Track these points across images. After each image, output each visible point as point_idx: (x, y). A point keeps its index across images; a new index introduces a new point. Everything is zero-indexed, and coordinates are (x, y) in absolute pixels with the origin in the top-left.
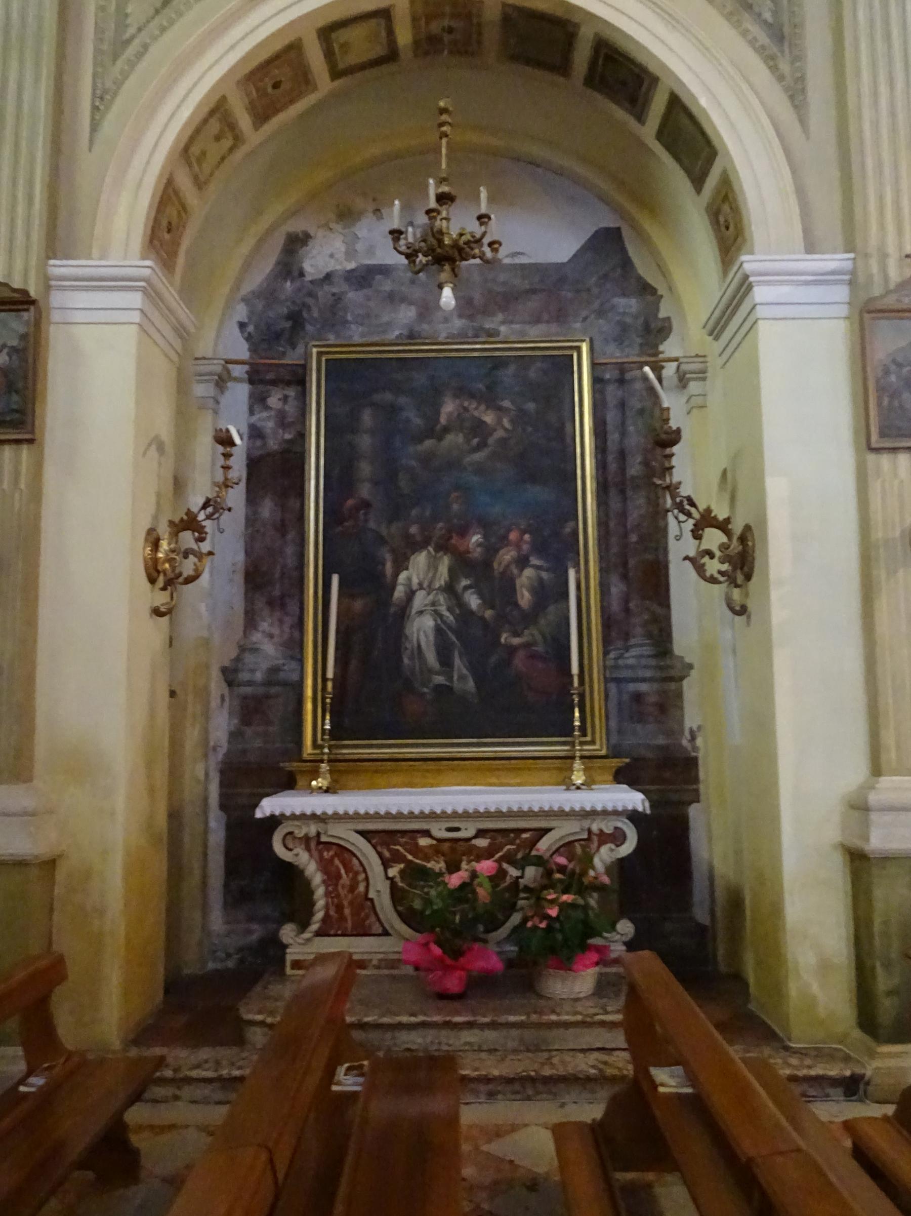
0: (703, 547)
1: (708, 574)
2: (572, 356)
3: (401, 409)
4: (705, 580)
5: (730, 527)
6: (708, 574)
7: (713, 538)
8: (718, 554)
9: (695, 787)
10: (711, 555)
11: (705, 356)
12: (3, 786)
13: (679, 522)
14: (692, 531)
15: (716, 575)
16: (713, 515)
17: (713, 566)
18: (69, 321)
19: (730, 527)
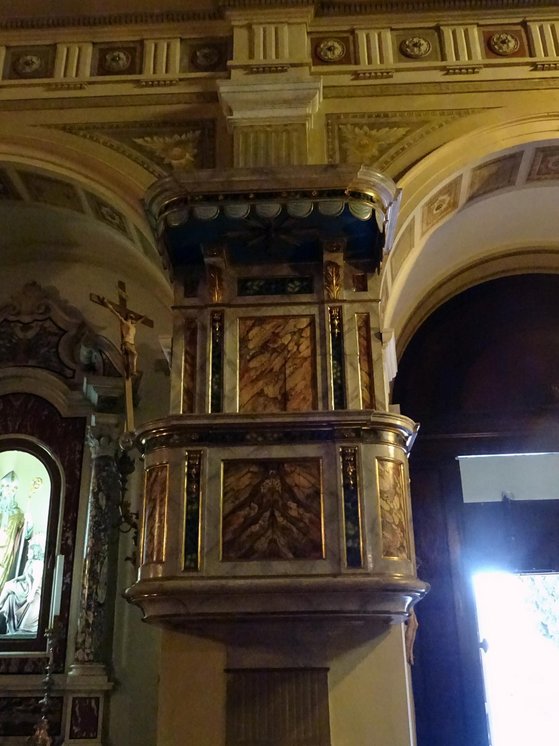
11: (26, 601)
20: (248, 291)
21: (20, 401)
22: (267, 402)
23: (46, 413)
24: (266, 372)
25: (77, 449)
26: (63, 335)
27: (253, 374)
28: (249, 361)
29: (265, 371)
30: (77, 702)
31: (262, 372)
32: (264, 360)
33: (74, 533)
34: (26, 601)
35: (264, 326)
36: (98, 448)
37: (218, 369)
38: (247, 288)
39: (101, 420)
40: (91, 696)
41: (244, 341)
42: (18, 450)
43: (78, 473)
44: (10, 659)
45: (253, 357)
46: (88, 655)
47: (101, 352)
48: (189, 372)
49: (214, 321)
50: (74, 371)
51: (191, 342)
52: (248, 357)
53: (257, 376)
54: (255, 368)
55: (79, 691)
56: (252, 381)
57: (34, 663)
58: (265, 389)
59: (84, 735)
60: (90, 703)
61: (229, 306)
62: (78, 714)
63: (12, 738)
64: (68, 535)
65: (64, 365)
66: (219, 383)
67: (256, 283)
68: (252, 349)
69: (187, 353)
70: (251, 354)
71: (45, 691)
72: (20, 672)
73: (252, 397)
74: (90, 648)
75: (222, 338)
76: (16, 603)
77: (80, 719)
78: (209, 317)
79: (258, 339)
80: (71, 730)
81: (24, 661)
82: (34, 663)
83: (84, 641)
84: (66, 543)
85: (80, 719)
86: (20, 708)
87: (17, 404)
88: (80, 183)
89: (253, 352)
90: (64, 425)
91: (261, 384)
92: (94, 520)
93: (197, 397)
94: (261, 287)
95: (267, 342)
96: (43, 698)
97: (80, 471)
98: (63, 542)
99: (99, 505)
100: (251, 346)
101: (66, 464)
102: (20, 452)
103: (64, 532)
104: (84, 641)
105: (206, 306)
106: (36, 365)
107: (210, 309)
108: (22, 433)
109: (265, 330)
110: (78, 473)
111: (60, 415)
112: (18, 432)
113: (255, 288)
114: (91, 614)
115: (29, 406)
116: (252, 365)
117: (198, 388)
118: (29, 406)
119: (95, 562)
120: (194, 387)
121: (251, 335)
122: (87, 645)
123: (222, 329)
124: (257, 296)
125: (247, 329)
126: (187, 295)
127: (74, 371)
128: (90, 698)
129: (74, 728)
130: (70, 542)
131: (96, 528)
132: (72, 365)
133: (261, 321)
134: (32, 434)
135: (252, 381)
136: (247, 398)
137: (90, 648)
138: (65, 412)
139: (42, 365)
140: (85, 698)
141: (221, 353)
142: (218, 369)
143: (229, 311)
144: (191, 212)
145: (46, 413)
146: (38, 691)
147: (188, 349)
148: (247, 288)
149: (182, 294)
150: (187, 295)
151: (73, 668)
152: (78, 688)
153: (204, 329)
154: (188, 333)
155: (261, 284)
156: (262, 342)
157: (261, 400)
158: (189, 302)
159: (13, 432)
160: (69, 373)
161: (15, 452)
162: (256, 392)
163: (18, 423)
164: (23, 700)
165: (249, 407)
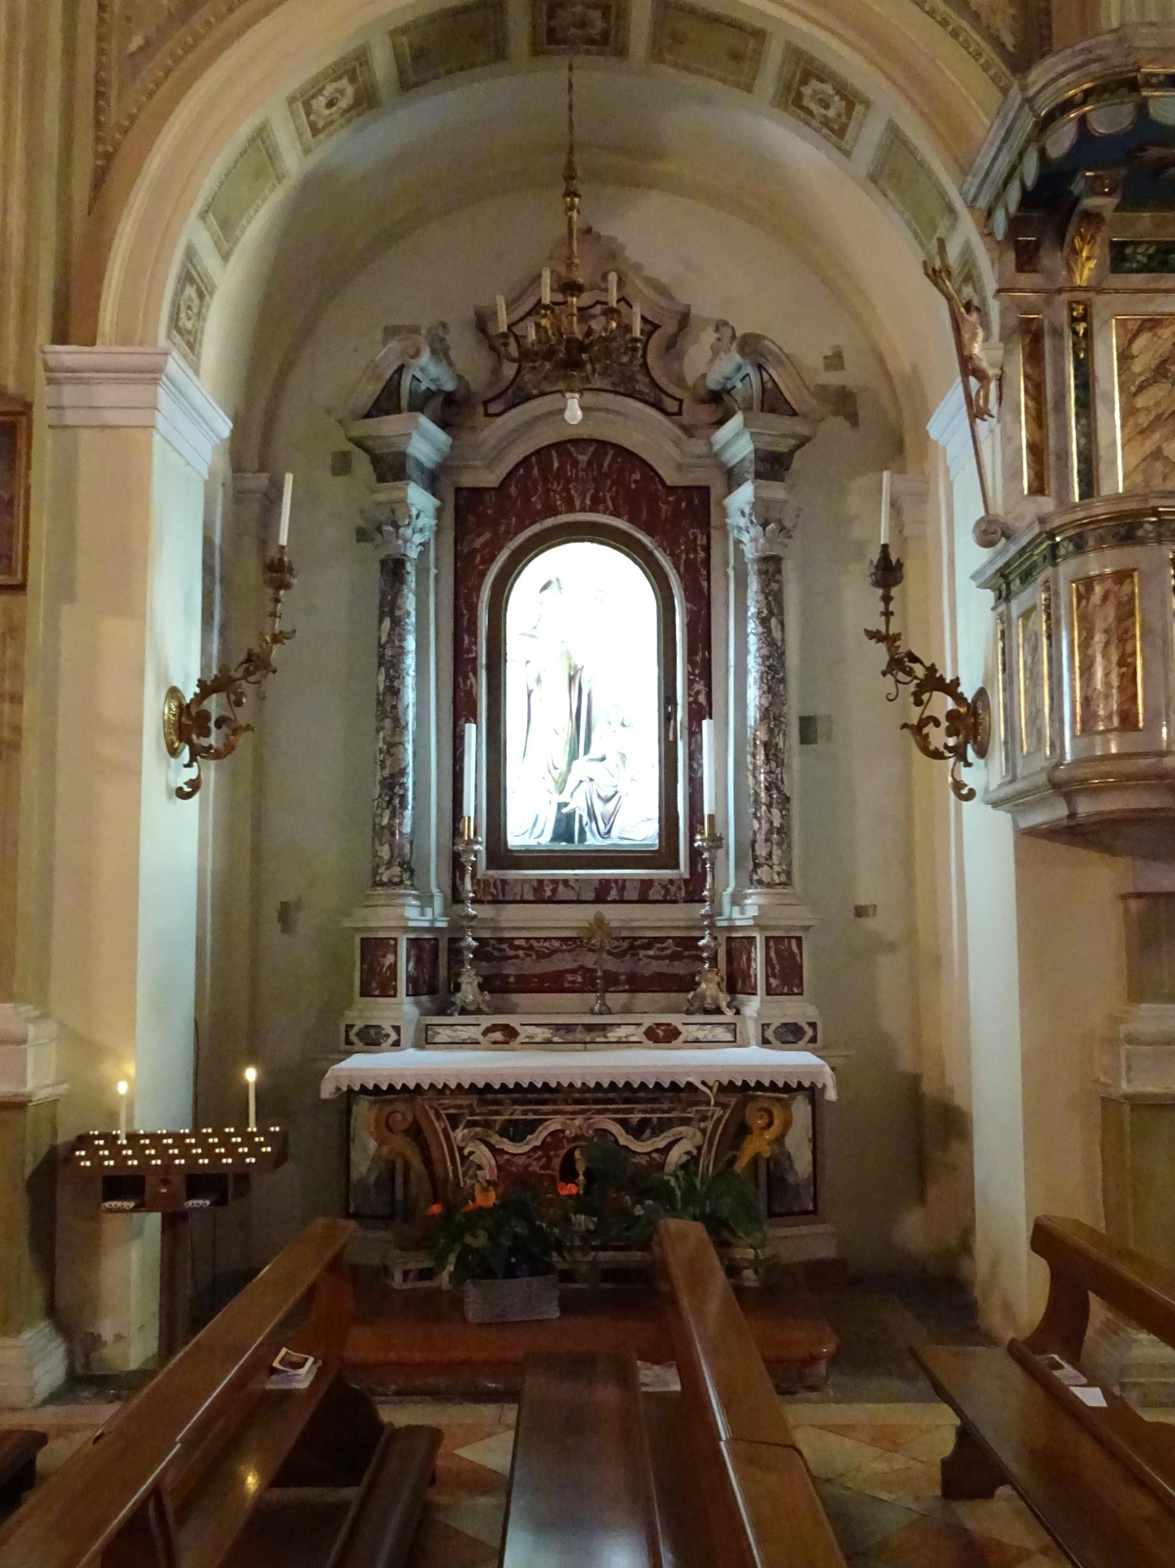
0: (927, 714)
1: (932, 747)
2: (488, 868)
3: (422, 907)
4: (927, 755)
5: (960, 690)
6: (932, 747)
7: (942, 704)
8: (945, 724)
9: (230, 1180)
10: (937, 724)
11: (616, 793)
12: (650, 3)
13: (897, 681)
14: (914, 694)
15: (942, 749)
16: (938, 675)
17: (939, 737)
18: (95, 404)
19: (960, 690)
20: (1127, 265)
21: (589, 454)
22: (1168, 470)
23: (637, 476)
24: (1166, 415)
25: (699, 543)
26: (652, 332)
27: (1144, 420)
28: (1135, 394)
29: (1163, 414)
30: (771, 943)
31: (1159, 417)
32: (1161, 394)
33: (709, 685)
34: (616, 793)
35: (1160, 331)
36: (762, 541)
37: (1086, 405)
38: (1125, 259)
39: (765, 494)
40: (792, 934)
41: (1125, 357)
42: (592, 541)
43: (705, 584)
44: (625, 880)
45: (1141, 388)
46: (779, 874)
47: (760, 368)
48: (1034, 413)
49: (1074, 320)
50: (681, 401)
51: (1034, 357)
52: (1133, 389)
53: (1151, 423)
54: (1147, 409)
55: (775, 928)
56: (1142, 432)
57: (664, 887)
58: (1165, 445)
59: (785, 991)
60: (789, 942)
61: (1100, 291)
62: (775, 962)
63: (641, 995)
64: (697, 687)
65: (661, 389)
66: (1089, 434)
67: (1141, 249)
68: (1140, 374)
69: (1027, 377)
70: (1137, 383)
71: (704, 928)
72: (643, 900)
73: (1144, 460)
74: (780, 864)
75: (1089, 350)
76: (599, 796)
77: (777, 967)
78: (1065, 312)
79: (1149, 355)
80: (768, 985)
81: (647, 884)
82: (664, 887)
83: (770, 854)
84: (696, 702)
85: (777, 967)
86: (651, 953)
87: (583, 459)
88: (781, 23)
89: (1142, 378)
90: (671, 499)
91: (1157, 436)
92: (767, 663)
93: (1052, 459)
94: (1150, 257)
95: (1165, 362)
96: (703, 938)
97: (708, 579)
98: (691, 699)
99: (773, 639)
100: (1137, 367)
101: (682, 569)
102: (595, 545)
103: (690, 683)
104: (770, 854)
105: (1060, 291)
106: (609, 387)
107: (1065, 297)
108: (597, 511)
109: (1160, 338)
110: (705, 584)
111: (662, 482)
112: (593, 509)
113: (1139, 257)
114: (775, 811)
115: (606, 464)
116: (1140, 402)
117: (1052, 443)
118: (606, 464)
119: (776, 731)
120: (1045, 438)
121: (1135, 349)
122: (775, 860)
123: (1088, 334)
124: (1145, 275)
125: (1130, 335)
126: (1020, 268)
127: (681, 401)
128: (789, 938)
129: (772, 980)
130: (702, 699)
131: (773, 677)
132: (678, 393)
133: (1151, 324)
134: (616, 514)
135: (1142, 432)
136: (1134, 462)
137: (780, 864)
138: (671, 477)
139: (621, 390)
140: (783, 938)
141: (1088, 378)
142: (1086, 405)
143: (1099, 300)
144: (1142, 108)
145: (637, 476)
146: (694, 928)
147: (1029, 370)
148: (1125, 259)
149: (1012, 266)
150: (1020, 268)
151: (752, 894)
152: (773, 923)
153: (1057, 334)
154: (1027, 341)
155: (1151, 251)
156: (1158, 361)
157: (1159, 465)
158: (1025, 280)
159: (583, 510)
160: (672, 406)
161: (587, 544)
162: (1148, 452)
163: (589, 496)
164: (651, 942)
165: (1138, 478)
